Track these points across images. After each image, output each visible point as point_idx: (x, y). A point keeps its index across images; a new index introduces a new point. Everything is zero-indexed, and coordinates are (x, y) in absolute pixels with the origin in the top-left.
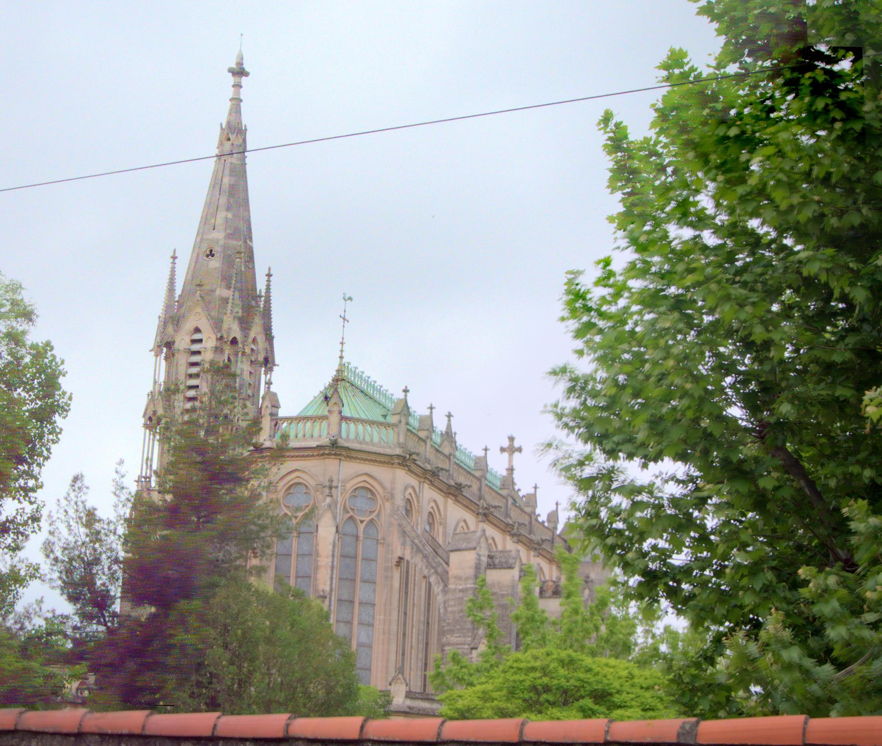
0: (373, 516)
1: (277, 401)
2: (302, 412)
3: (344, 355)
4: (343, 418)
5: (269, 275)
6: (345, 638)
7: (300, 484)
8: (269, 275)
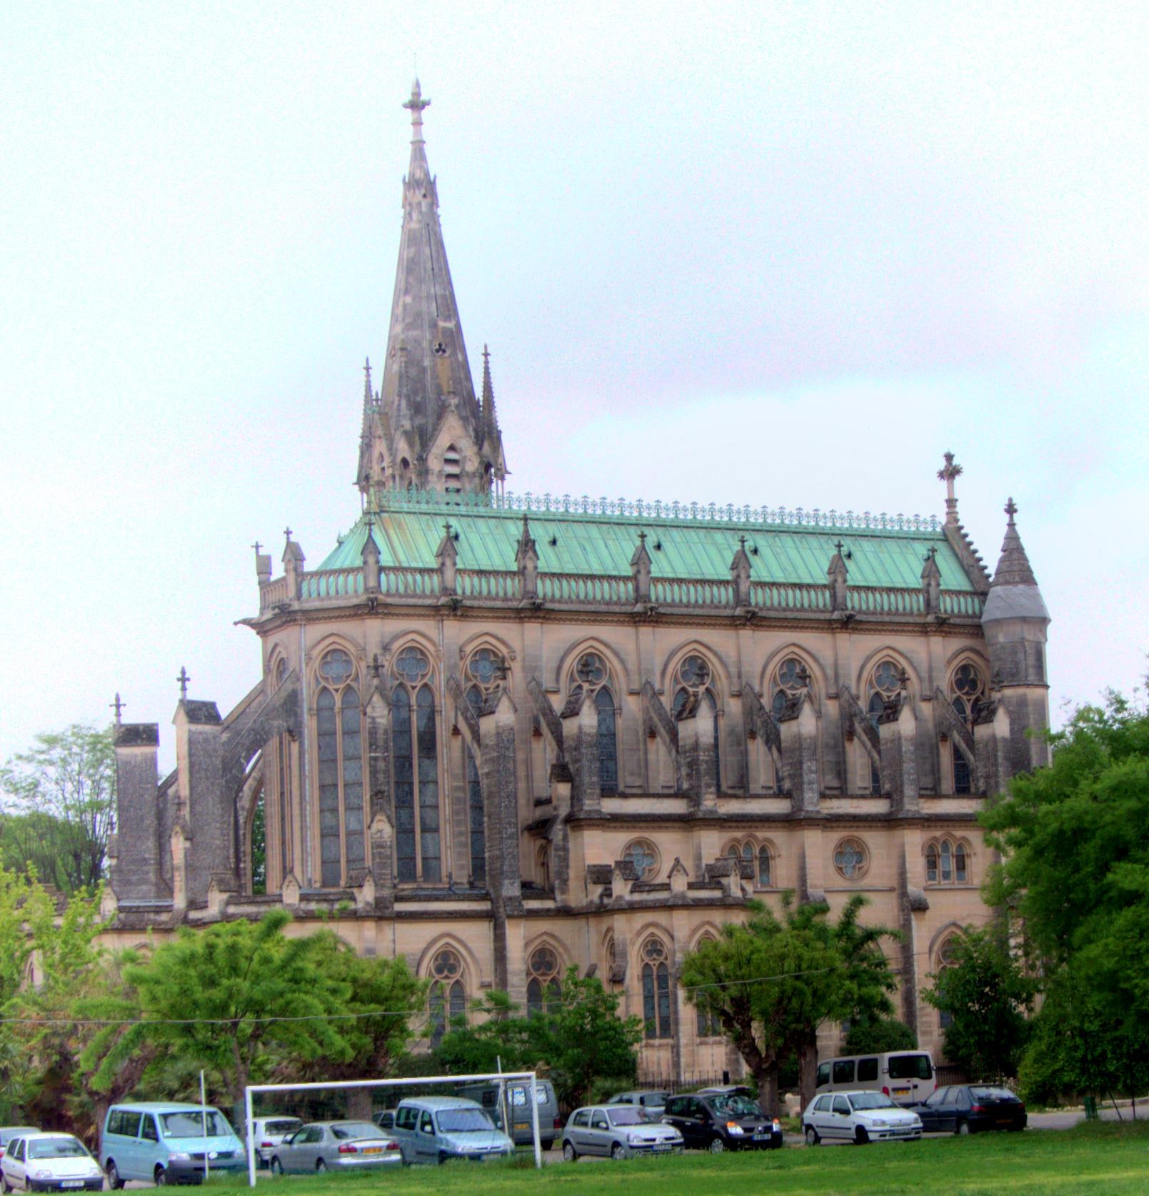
0: (425, 680)
2: (325, 563)
3: (1006, 517)
4: (381, 569)
5: (486, 355)
6: (332, 827)
8: (486, 355)
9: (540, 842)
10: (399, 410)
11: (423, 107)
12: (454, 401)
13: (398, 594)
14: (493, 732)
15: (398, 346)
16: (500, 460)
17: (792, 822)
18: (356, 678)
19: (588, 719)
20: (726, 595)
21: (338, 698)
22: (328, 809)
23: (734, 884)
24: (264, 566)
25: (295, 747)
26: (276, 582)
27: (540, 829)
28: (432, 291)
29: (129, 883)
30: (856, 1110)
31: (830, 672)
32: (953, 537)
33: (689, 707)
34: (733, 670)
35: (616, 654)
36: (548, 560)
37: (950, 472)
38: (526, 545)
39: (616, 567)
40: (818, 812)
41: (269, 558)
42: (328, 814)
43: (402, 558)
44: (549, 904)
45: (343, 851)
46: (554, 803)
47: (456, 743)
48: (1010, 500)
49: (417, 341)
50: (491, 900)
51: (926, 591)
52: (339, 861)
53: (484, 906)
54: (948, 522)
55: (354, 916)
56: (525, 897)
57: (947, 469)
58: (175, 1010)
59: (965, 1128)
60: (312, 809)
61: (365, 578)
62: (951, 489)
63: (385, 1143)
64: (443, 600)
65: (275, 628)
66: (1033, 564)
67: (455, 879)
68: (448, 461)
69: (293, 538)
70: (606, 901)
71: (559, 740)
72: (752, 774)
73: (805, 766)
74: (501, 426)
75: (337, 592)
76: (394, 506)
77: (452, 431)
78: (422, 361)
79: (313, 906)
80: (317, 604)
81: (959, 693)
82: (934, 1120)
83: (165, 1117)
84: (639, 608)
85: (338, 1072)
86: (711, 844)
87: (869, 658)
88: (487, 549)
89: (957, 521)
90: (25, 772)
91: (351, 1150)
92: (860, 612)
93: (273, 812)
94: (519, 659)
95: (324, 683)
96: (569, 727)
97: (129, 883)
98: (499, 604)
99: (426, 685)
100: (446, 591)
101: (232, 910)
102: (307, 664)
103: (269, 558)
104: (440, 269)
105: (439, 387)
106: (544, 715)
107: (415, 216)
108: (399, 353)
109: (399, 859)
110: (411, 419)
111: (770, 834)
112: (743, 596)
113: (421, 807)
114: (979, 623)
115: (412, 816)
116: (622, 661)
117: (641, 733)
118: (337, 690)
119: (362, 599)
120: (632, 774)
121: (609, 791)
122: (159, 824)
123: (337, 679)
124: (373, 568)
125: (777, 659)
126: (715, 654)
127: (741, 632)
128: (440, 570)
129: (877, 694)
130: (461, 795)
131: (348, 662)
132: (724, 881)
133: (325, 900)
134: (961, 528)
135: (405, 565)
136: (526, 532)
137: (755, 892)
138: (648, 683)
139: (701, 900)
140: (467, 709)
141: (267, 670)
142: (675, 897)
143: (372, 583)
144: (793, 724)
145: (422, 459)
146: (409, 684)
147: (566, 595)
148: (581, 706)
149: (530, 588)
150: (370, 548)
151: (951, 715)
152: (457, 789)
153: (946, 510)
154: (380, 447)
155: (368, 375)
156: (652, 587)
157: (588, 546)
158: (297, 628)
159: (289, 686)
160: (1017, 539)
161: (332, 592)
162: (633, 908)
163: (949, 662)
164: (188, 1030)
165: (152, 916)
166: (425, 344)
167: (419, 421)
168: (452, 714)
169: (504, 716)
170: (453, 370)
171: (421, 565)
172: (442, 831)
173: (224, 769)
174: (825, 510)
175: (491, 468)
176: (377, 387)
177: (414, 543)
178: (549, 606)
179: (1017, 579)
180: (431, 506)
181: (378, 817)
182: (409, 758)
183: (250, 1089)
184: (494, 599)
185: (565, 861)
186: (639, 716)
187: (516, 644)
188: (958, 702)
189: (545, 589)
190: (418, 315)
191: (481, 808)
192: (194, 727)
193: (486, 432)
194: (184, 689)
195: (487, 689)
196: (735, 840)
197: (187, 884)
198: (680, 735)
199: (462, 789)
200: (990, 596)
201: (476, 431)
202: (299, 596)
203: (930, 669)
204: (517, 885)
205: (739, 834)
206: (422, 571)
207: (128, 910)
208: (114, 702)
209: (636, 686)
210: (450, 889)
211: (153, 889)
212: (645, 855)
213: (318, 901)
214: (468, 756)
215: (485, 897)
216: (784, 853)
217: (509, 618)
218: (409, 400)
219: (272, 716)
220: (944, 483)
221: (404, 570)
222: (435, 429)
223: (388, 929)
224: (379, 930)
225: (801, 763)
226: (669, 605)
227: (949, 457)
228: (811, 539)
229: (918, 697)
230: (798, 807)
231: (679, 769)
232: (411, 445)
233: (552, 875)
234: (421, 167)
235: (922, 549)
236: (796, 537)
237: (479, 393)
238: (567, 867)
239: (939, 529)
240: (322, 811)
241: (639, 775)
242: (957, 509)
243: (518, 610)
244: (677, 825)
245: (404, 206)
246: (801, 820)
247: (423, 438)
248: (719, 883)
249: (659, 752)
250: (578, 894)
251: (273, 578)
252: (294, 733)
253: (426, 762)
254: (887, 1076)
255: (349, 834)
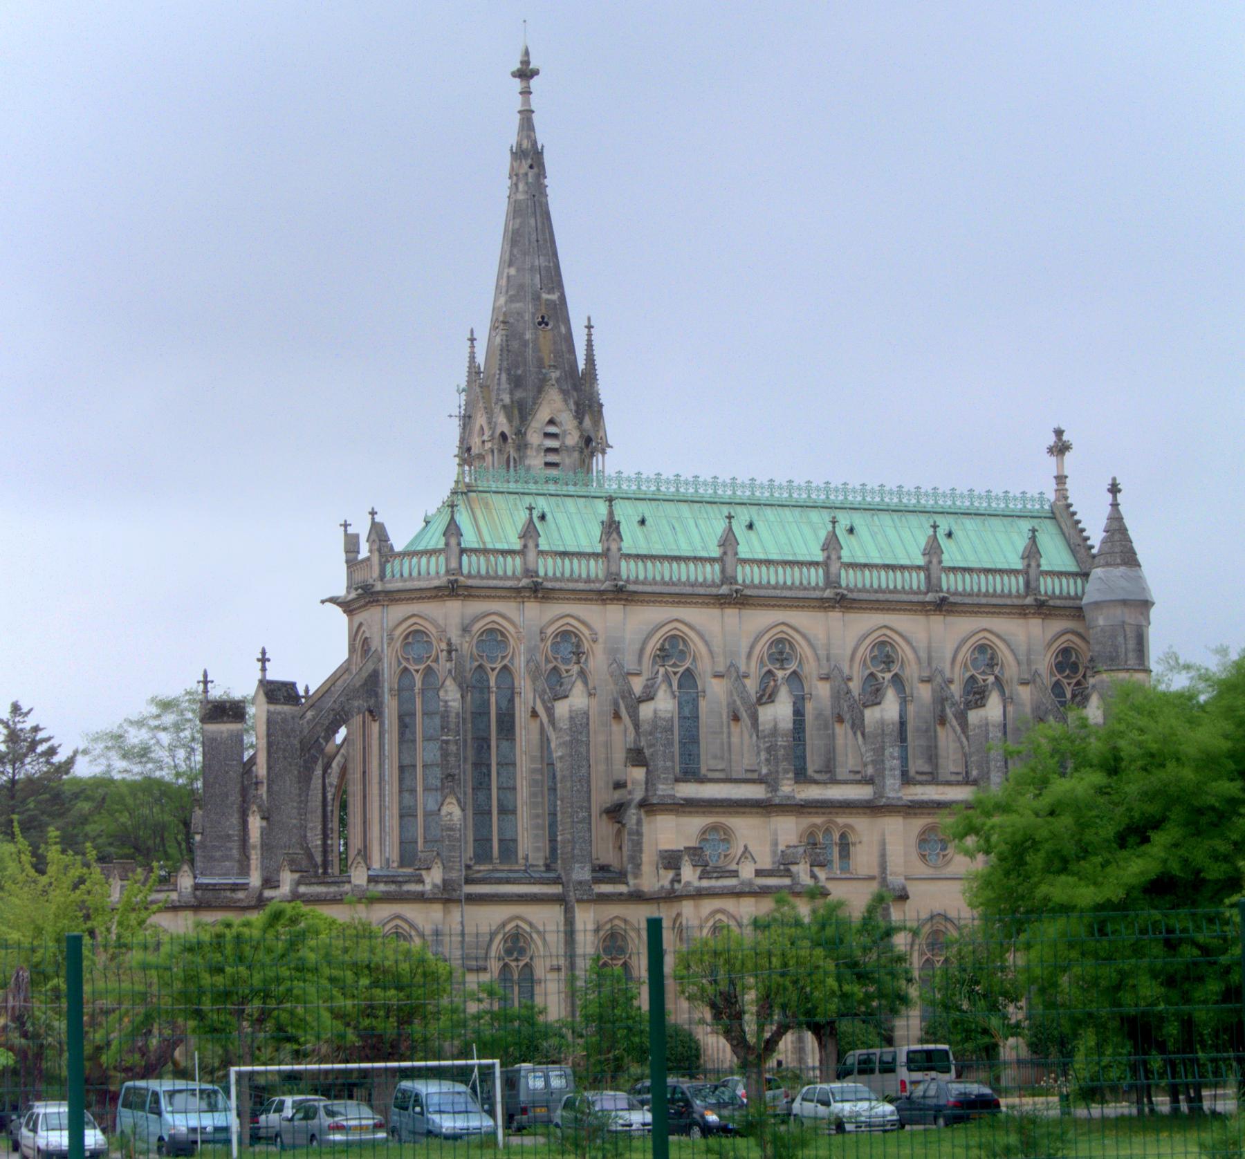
1: (386, 536)
2: (412, 543)
3: (1110, 496)
4: (463, 551)
5: (589, 327)
7: (417, 631)
8: (589, 327)
9: (617, 826)
10: (499, 384)
11: (532, 76)
12: (555, 374)
13: (479, 576)
14: (567, 715)
15: (501, 319)
16: (601, 434)
17: (872, 808)
18: (436, 660)
19: (664, 704)
20: (815, 577)
21: (418, 678)
22: (405, 788)
23: (802, 871)
24: (351, 544)
25: (375, 727)
26: (363, 561)
27: (616, 812)
28: (537, 263)
29: (212, 858)
30: (835, 1101)
31: (923, 655)
32: (1062, 515)
33: (768, 691)
34: (822, 653)
35: (702, 636)
36: (632, 539)
37: (1060, 448)
38: (610, 526)
39: (705, 548)
40: (900, 798)
41: (357, 536)
42: (406, 795)
43: (487, 539)
44: (622, 889)
45: (420, 831)
46: (629, 786)
47: (534, 726)
48: (1114, 479)
49: (520, 314)
50: (562, 883)
51: (1026, 572)
52: (416, 842)
53: (556, 889)
54: (1057, 499)
55: (421, 898)
56: (597, 881)
57: (1056, 445)
58: (185, 996)
59: (941, 1121)
60: (392, 787)
61: (447, 560)
62: (1060, 465)
63: (371, 1122)
64: (524, 582)
65: (360, 607)
66: (1136, 546)
67: (531, 861)
68: (547, 435)
69: (378, 519)
70: (676, 886)
71: (637, 725)
72: (840, 758)
73: (887, 753)
74: (604, 399)
75: (419, 573)
76: (482, 485)
77: (553, 405)
78: (524, 334)
79: (382, 887)
80: (399, 585)
81: (1059, 677)
82: (912, 1112)
83: (172, 1094)
84: (724, 590)
85: (363, 1054)
86: (788, 829)
87: (964, 641)
88: (573, 529)
89: (1066, 498)
90: (136, 737)
91: (339, 1128)
92: (956, 593)
93: (355, 789)
94: (600, 640)
95: (404, 664)
96: (646, 711)
97: (212, 858)
98: (581, 586)
99: (505, 667)
100: (529, 572)
101: (302, 889)
102: (389, 644)
103: (357, 536)
104: (545, 240)
105: (540, 364)
106: (623, 698)
107: (521, 186)
108: (502, 326)
109: (475, 840)
110: (511, 393)
111: (851, 820)
112: (833, 578)
113: (499, 789)
114: (1081, 602)
115: (489, 798)
116: (707, 643)
117: (725, 717)
118: (417, 671)
119: (442, 581)
120: (715, 757)
121: (691, 774)
122: (244, 801)
123: (418, 660)
124: (456, 550)
125: (868, 641)
126: (804, 636)
127: (831, 614)
128: (522, 552)
129: (972, 677)
130: (539, 777)
131: (429, 643)
132: (794, 868)
133: (393, 882)
134: (1071, 505)
135: (490, 546)
136: (611, 513)
137: (827, 879)
138: (732, 665)
139: (768, 887)
140: (544, 691)
141: (352, 649)
142: (742, 884)
143: (454, 564)
144: (877, 709)
145: (520, 434)
146: (488, 666)
147: (650, 577)
148: (656, 691)
149: (614, 569)
150: (452, 529)
151: (1049, 700)
152: (533, 771)
153: (1055, 487)
154: (480, 420)
155: (472, 347)
156: (739, 568)
157: (676, 526)
158: (380, 608)
159: (370, 667)
160: (1120, 519)
161: (415, 573)
162: (700, 894)
163: (1050, 645)
164: (199, 1014)
165: (228, 893)
166: (527, 317)
167: (519, 394)
168: (531, 696)
169: (577, 699)
170: (555, 343)
171: (506, 547)
172: (519, 812)
173: (302, 750)
174: (927, 487)
175: (591, 445)
176: (481, 359)
177: (497, 525)
178: (631, 587)
179: (1119, 561)
180: (519, 485)
181: (448, 800)
182: (487, 740)
183: (497, 1061)
184: (577, 581)
185: (638, 846)
186: (724, 700)
187: (598, 625)
188: (1057, 684)
189: (628, 570)
190: (521, 287)
191: (555, 790)
192: (272, 707)
193: (586, 404)
194: (264, 669)
195: (567, 671)
196: (815, 825)
197: (262, 863)
198: (761, 719)
199: (541, 771)
200: (1091, 578)
201: (577, 404)
202: (382, 577)
203: (1029, 652)
204: (588, 867)
205: (818, 820)
206: (505, 553)
207: (206, 888)
208: (202, 679)
209: (721, 668)
210: (525, 871)
211: (236, 865)
212: (723, 840)
213: (386, 883)
214: (544, 741)
215: (556, 881)
216: (865, 839)
217: (591, 600)
218: (509, 374)
219: (356, 692)
220: (1054, 459)
221: (485, 551)
222: (534, 403)
223: (456, 913)
224: (446, 912)
225: (883, 749)
226: (756, 587)
227: (1059, 433)
228: (911, 517)
229: (1015, 680)
230: (879, 794)
231: (758, 754)
232: (510, 419)
233: (625, 859)
234: (529, 137)
235: (1026, 525)
236: (895, 515)
237: (581, 365)
238: (641, 851)
239: (1046, 507)
240: (401, 791)
241: (722, 758)
242: (1067, 486)
243: (601, 592)
244: (754, 810)
245: (510, 177)
246: (882, 806)
247: (521, 412)
248: (788, 870)
249: (740, 736)
250: (651, 879)
251: (360, 557)
252: (374, 713)
253: (505, 744)
254: (905, 1069)
255: (427, 814)
